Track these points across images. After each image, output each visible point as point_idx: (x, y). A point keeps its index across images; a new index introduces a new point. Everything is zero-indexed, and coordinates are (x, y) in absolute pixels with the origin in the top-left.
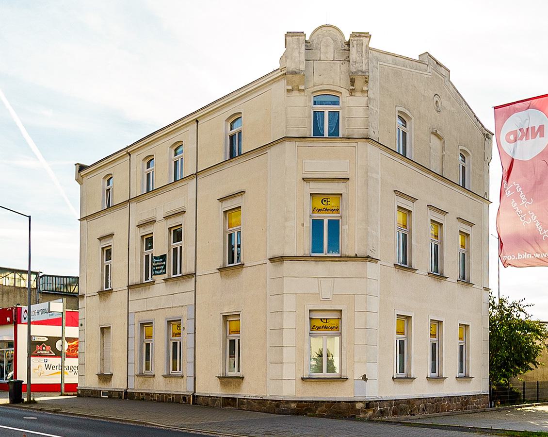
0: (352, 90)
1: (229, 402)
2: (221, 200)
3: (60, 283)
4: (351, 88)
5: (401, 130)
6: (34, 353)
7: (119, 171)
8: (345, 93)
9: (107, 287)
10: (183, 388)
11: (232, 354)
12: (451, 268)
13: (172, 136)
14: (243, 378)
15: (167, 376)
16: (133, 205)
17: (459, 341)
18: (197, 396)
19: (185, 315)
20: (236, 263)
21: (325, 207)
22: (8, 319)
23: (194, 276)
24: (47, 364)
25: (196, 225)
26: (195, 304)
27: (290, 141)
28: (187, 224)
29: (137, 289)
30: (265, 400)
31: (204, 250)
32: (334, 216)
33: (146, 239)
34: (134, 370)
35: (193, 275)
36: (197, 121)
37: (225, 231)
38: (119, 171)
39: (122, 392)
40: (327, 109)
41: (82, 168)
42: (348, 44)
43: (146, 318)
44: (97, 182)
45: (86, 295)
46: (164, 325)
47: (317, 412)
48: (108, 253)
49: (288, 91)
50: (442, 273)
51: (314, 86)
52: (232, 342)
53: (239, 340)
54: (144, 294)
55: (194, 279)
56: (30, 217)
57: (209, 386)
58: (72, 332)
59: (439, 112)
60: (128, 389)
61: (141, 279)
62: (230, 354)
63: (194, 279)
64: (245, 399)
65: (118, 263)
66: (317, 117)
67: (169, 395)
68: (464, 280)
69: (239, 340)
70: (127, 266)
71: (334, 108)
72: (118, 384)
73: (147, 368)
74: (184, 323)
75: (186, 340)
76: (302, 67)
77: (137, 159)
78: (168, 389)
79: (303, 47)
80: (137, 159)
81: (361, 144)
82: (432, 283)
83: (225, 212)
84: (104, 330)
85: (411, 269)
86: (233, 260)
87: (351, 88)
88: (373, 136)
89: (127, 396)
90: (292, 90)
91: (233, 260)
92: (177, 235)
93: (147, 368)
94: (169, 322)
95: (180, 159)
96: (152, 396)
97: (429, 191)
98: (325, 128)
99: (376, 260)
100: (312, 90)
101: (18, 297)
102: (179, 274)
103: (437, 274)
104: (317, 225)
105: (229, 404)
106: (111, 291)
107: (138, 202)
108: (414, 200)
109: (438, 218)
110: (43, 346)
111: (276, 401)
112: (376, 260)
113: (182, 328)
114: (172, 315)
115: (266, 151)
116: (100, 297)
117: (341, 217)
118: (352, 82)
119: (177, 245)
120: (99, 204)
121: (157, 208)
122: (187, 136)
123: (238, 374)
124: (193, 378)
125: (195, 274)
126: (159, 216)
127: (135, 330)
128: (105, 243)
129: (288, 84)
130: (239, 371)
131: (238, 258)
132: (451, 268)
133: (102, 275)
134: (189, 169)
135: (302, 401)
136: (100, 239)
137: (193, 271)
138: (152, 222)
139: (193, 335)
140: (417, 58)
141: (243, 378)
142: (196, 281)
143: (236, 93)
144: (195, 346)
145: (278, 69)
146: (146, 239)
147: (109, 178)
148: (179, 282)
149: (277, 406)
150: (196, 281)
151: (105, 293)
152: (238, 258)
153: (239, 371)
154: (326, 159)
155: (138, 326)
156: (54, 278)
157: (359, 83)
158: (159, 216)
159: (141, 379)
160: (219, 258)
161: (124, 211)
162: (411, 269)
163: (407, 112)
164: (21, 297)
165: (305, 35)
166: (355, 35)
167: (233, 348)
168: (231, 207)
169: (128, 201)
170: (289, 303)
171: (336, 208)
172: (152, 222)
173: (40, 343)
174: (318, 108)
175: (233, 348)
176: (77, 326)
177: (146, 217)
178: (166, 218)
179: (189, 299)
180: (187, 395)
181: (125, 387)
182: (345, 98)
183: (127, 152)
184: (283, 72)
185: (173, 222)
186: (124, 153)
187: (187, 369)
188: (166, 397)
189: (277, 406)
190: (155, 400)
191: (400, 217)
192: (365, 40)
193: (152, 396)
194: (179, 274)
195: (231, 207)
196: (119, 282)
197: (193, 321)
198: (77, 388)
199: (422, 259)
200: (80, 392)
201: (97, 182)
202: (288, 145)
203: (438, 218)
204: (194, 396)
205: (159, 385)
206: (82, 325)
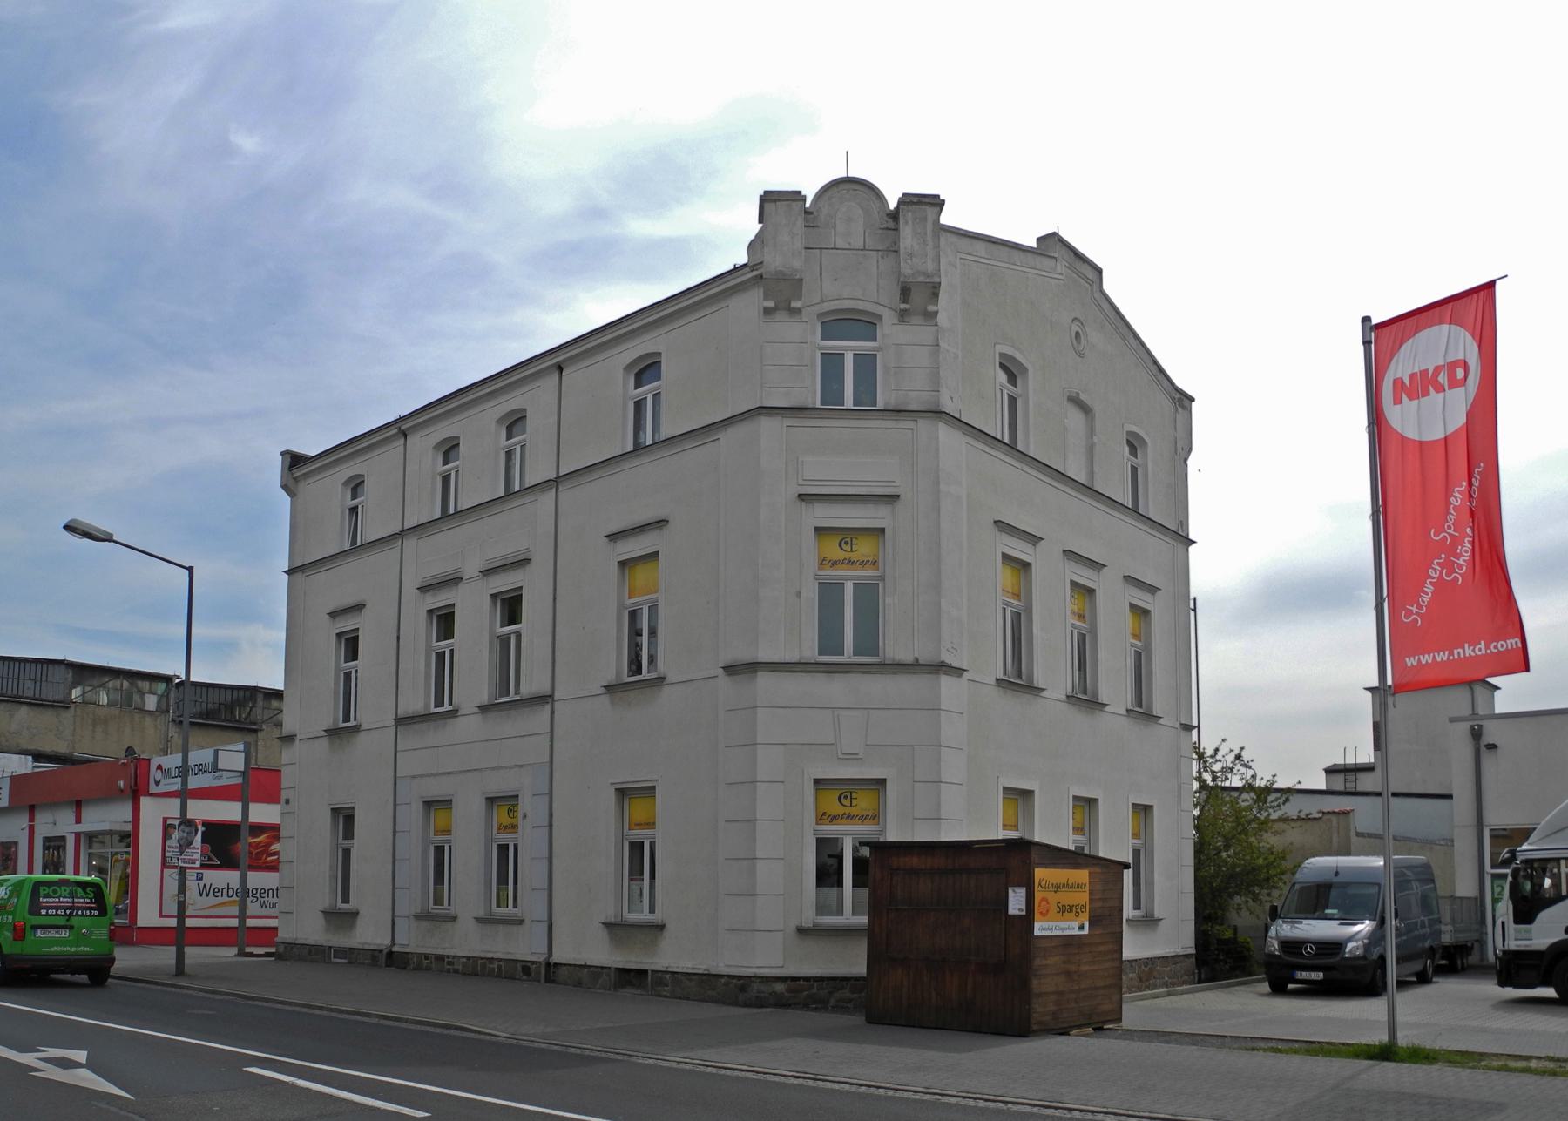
0: (905, 310)
1: (631, 978)
4: (903, 306)
7: (378, 469)
8: (888, 317)
9: (346, 719)
10: (525, 946)
11: (636, 872)
12: (1115, 687)
13: (501, 399)
14: (661, 927)
15: (486, 921)
16: (410, 543)
17: (1131, 841)
18: (556, 965)
20: (645, 675)
21: (847, 810)
26: (551, 762)
27: (770, 415)
28: (534, 587)
31: (574, 639)
34: (410, 903)
35: (545, 699)
36: (560, 369)
38: (378, 469)
40: (849, 349)
41: (294, 461)
42: (894, 215)
43: (436, 790)
44: (329, 489)
46: (479, 805)
47: (832, 1002)
48: (351, 645)
49: (767, 311)
50: (1095, 694)
52: (637, 848)
53: (652, 845)
54: (433, 736)
55: (548, 707)
56: (190, 569)
57: (584, 946)
58: (262, 813)
59: (1081, 355)
60: (393, 944)
61: (427, 705)
62: (630, 874)
66: (832, 364)
68: (1142, 713)
69: (652, 845)
70: (391, 678)
72: (370, 934)
73: (438, 900)
74: (525, 804)
75: (529, 841)
76: (797, 263)
79: (800, 222)
80: (423, 444)
81: (923, 426)
82: (1078, 719)
83: (622, 564)
84: (345, 819)
86: (638, 674)
87: (903, 306)
88: (948, 406)
89: (393, 960)
91: (638, 674)
92: (511, 607)
93: (438, 900)
94: (491, 801)
95: (518, 448)
96: (450, 963)
97: (1061, 521)
98: (847, 396)
99: (959, 672)
103: (1086, 699)
104: (830, 594)
105: (629, 984)
106: (356, 729)
108: (1035, 540)
109: (1085, 577)
112: (959, 672)
113: (520, 816)
114: (500, 784)
117: (883, 578)
118: (905, 293)
121: (466, 548)
123: (650, 917)
124: (545, 926)
127: (412, 816)
128: (345, 625)
129: (766, 298)
130: (652, 910)
131: (652, 659)
132: (1115, 687)
133: (336, 693)
134: (539, 470)
135: (798, 979)
136: (334, 615)
137: (545, 688)
138: (453, 581)
140: (1034, 245)
141: (661, 927)
142: (553, 712)
147: (356, 486)
149: (743, 989)
150: (553, 712)
151: (342, 733)
152: (652, 659)
153: (652, 910)
154: (848, 458)
155: (417, 809)
157: (917, 297)
158: (471, 568)
159: (425, 924)
160: (612, 665)
161: (391, 554)
163: (1018, 356)
165: (804, 199)
166: (908, 200)
167: (639, 859)
168: (637, 550)
172: (453, 581)
175: (639, 859)
176: (278, 801)
177: (437, 569)
178: (486, 573)
182: (889, 329)
185: (503, 583)
187: (531, 905)
188: (483, 966)
189: (743, 989)
190: (456, 971)
191: (1004, 577)
192: (930, 211)
193: (450, 963)
195: (637, 550)
196: (374, 710)
199: (1053, 668)
200: (282, 949)
202: (766, 424)
203: (1085, 577)
205: (466, 941)
206: (287, 801)
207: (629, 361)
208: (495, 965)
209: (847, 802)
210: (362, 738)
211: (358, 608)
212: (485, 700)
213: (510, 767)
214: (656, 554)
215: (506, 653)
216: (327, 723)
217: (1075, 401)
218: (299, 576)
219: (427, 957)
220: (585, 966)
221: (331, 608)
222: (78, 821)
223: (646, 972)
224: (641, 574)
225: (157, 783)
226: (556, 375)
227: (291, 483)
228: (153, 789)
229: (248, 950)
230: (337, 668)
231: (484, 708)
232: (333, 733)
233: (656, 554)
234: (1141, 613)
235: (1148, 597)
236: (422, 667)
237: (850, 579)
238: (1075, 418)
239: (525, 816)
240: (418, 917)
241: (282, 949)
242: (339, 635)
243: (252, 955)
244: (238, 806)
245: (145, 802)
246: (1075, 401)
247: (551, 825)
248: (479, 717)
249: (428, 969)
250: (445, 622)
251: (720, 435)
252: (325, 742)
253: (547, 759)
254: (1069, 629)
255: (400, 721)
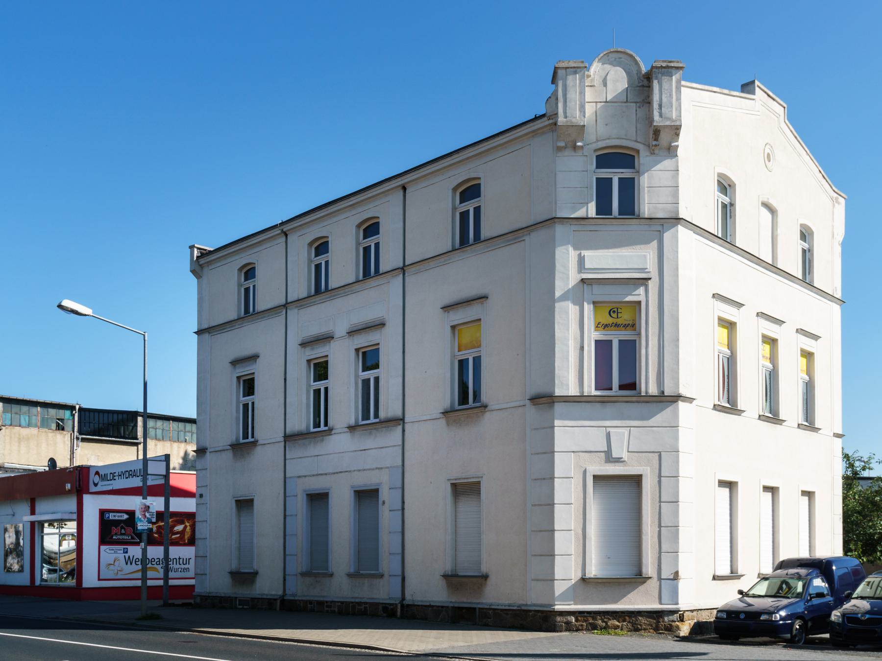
2: (447, 308)
3: (101, 421)
4: (654, 143)
5: (720, 201)
6: (108, 540)
16: (293, 313)
18: (408, 605)
19: (384, 481)
21: (615, 321)
22: (68, 486)
23: (401, 422)
24: (127, 555)
25: (404, 345)
29: (300, 442)
30: (524, 610)
32: (626, 335)
33: (315, 364)
35: (400, 421)
36: (404, 188)
37: (453, 356)
39: (276, 600)
40: (615, 175)
45: (209, 450)
48: (249, 386)
51: (597, 141)
63: (400, 427)
64: (490, 609)
65: (266, 399)
67: (360, 604)
71: (626, 173)
77: (300, 244)
78: (357, 595)
80: (300, 244)
83: (453, 327)
85: (739, 412)
90: (565, 148)
92: (369, 359)
96: (327, 606)
99: (690, 400)
100: (595, 146)
101: (44, 445)
102: (373, 420)
106: (255, 443)
107: (301, 307)
110: (122, 528)
111: (542, 612)
115: (523, 236)
116: (235, 455)
119: (371, 374)
120: (231, 309)
121: (337, 316)
122: (387, 212)
124: (400, 579)
125: (403, 419)
126: (340, 330)
127: (299, 506)
133: (238, 418)
137: (399, 413)
138: (326, 338)
139: (400, 512)
142: (404, 431)
143: (471, 150)
144: (285, 518)
145: (543, 116)
146: (315, 364)
147: (249, 272)
148: (374, 432)
150: (404, 431)
156: (97, 414)
158: (340, 330)
160: (444, 394)
161: (278, 321)
162: (739, 412)
164: (47, 445)
169: (284, 306)
170: (563, 465)
171: (631, 323)
172: (326, 338)
173: (117, 523)
174: (605, 173)
178: (351, 333)
179: (391, 457)
180: (391, 604)
181: (280, 593)
182: (643, 158)
183: (283, 230)
184: (551, 121)
185: (362, 341)
186: (277, 231)
190: (334, 612)
193: (330, 607)
194: (373, 420)
196: (269, 428)
197: (400, 491)
198: (194, 594)
199: (751, 394)
200: (198, 600)
201: (227, 277)
204: (402, 606)
207: (455, 183)
208: (363, 607)
209: (614, 315)
210: (258, 450)
211: (254, 358)
212: (352, 422)
213: (373, 469)
214: (480, 320)
215: (369, 394)
216: (232, 439)
217: (766, 205)
218: (206, 336)
219: (311, 602)
220: (430, 606)
221: (232, 357)
222: (33, 512)
223: (474, 609)
224: (467, 335)
225: (96, 485)
226: (401, 192)
227: (197, 268)
228: (93, 489)
229: (171, 601)
230: (238, 402)
231: (352, 428)
232: (236, 447)
233: (480, 320)
234: (808, 355)
235: (811, 342)
236: (304, 401)
237: (615, 338)
238: (766, 215)
239: (384, 503)
240: (303, 574)
241: (198, 600)
242: (238, 378)
243: (174, 605)
244: (162, 500)
245: (87, 498)
246: (766, 205)
247: (403, 509)
248: (349, 434)
249: (312, 611)
250: (321, 370)
251: (526, 238)
252: (229, 454)
253: (400, 463)
254: (761, 368)
255: (289, 438)
